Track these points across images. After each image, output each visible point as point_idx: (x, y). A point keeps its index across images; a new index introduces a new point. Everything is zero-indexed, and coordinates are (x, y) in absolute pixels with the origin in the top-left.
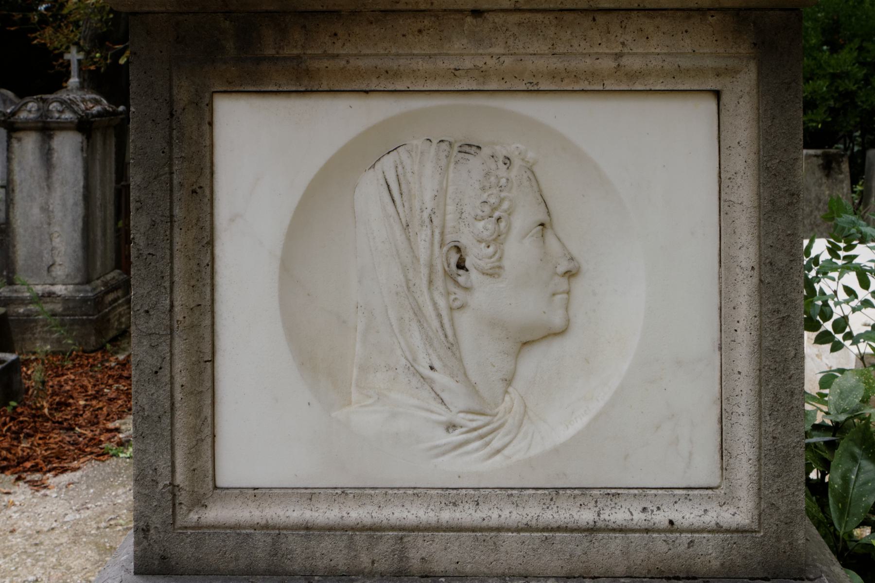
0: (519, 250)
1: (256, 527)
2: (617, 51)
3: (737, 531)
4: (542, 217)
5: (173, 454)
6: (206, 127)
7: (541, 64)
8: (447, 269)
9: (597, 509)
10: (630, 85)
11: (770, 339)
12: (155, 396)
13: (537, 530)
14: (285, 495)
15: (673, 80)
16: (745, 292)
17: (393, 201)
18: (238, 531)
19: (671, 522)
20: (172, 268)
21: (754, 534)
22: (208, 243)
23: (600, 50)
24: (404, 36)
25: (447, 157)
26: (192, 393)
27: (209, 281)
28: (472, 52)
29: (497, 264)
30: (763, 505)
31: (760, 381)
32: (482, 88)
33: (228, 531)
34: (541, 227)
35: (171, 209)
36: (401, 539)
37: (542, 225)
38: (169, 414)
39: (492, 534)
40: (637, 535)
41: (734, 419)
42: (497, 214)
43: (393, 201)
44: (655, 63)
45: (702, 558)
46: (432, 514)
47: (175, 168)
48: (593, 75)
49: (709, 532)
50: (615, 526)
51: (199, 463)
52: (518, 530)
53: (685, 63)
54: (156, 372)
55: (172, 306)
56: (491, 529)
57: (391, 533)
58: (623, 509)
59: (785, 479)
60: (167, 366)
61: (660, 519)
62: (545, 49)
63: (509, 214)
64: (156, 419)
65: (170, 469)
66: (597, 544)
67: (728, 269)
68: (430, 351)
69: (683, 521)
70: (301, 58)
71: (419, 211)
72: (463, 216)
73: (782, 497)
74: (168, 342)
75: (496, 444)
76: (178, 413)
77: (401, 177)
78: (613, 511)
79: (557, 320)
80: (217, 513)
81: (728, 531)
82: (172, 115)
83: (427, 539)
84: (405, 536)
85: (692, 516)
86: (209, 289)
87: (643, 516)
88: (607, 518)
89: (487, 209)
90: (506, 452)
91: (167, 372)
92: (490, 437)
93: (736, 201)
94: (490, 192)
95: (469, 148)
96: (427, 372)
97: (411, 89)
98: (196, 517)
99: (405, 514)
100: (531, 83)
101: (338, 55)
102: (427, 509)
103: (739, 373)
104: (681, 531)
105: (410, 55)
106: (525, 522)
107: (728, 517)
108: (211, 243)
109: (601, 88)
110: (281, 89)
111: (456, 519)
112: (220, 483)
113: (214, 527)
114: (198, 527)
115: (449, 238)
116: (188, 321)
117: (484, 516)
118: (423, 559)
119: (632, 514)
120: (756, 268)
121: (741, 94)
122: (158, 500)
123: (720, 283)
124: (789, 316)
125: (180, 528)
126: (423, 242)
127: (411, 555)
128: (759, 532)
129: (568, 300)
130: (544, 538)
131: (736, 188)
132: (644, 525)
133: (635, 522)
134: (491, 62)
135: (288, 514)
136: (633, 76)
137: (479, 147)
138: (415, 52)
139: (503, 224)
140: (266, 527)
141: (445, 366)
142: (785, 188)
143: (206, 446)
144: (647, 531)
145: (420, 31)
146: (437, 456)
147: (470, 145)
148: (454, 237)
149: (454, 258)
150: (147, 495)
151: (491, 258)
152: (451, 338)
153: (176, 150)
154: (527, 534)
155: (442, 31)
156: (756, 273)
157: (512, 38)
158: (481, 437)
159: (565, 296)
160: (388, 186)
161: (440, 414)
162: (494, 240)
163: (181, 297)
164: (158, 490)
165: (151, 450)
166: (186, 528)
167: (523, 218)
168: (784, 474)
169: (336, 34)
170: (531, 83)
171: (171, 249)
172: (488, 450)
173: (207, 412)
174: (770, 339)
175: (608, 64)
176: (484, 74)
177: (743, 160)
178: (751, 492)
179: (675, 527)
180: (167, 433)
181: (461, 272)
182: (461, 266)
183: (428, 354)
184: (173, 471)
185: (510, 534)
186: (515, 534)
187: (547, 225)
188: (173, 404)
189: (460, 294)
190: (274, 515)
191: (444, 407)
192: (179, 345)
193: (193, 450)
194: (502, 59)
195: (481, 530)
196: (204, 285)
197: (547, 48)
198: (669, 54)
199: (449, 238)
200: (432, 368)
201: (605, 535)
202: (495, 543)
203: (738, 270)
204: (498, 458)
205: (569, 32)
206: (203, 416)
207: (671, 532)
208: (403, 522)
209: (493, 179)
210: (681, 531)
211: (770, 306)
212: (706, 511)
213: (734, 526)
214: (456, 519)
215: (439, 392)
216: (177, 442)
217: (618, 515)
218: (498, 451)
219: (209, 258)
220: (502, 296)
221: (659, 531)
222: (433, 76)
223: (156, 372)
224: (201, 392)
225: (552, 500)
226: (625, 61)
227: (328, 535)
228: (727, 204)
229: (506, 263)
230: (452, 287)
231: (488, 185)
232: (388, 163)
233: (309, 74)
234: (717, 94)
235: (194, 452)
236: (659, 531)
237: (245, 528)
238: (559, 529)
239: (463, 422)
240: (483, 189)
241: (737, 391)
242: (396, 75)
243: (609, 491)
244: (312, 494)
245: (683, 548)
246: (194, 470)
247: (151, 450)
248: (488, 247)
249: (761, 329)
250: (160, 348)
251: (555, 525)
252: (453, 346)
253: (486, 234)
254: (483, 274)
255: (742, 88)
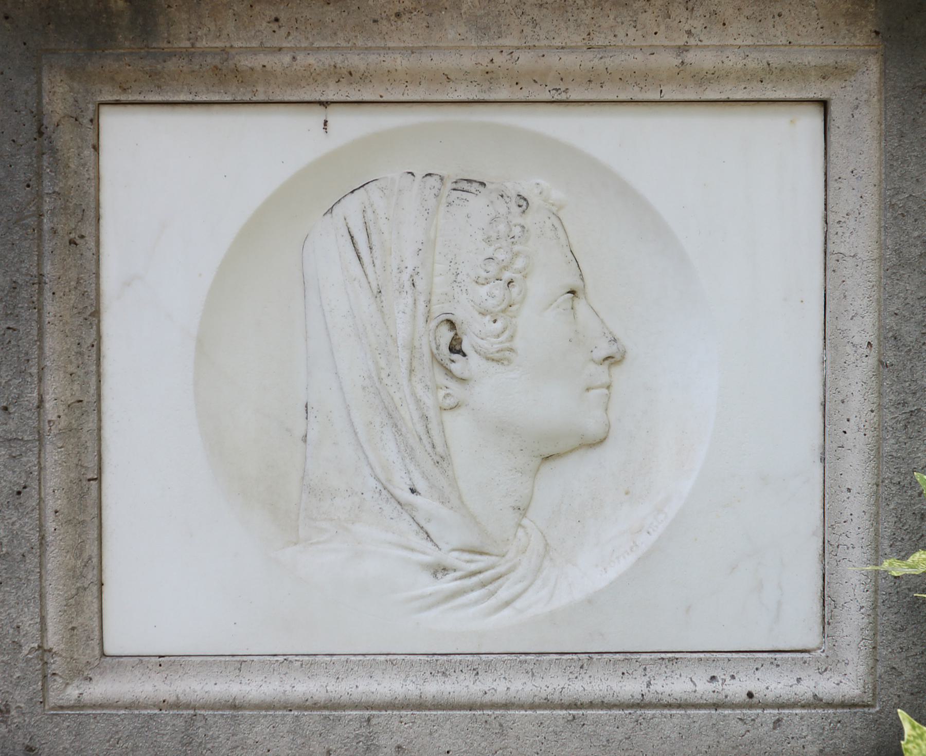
0: (539, 323)
1: (163, 705)
2: (681, 43)
3: (843, 705)
4: (572, 281)
5: (42, 607)
6: (88, 152)
7: (570, 60)
8: (435, 351)
9: (646, 679)
10: (701, 92)
11: (893, 441)
12: (18, 525)
13: (562, 706)
14: (201, 664)
15: (760, 84)
16: (858, 377)
17: (359, 258)
18: (136, 712)
19: (750, 695)
20: (41, 348)
21: (866, 710)
22: (92, 315)
23: (656, 41)
24: (375, 21)
25: (436, 196)
26: (69, 522)
27: (94, 368)
28: (474, 44)
29: (507, 345)
30: (880, 670)
31: (877, 500)
32: (486, 97)
33: (123, 712)
34: (570, 295)
35: (39, 265)
36: (369, 720)
37: (572, 292)
38: (37, 551)
39: (498, 712)
40: (702, 712)
41: (841, 552)
42: (507, 275)
43: (359, 258)
44: (733, 60)
45: (792, 741)
46: (411, 687)
47: (46, 207)
48: (644, 77)
49: (803, 707)
50: (671, 700)
51: (80, 620)
52: (533, 706)
53: (777, 59)
54: (19, 493)
55: (41, 401)
56: (494, 706)
57: (354, 713)
58: (683, 678)
59: (910, 634)
60: (35, 484)
61: (736, 689)
62: (577, 39)
63: (525, 277)
64: (19, 558)
65: (38, 626)
66: (644, 724)
67: (835, 347)
68: (412, 468)
69: (766, 692)
70: (227, 53)
71: (395, 271)
72: (459, 278)
73: (907, 658)
74: (36, 450)
75: (504, 594)
76: (50, 549)
77: (371, 225)
78: (669, 681)
79: (592, 425)
80: (102, 688)
81: (830, 705)
82: (41, 133)
83: (404, 720)
84: (374, 716)
85: (780, 686)
86: (94, 379)
87: (712, 686)
88: (660, 689)
89: (493, 268)
90: (518, 604)
91: (34, 493)
92: (496, 584)
93: (848, 254)
94: (498, 245)
95: (467, 185)
96: (407, 496)
97: (384, 99)
98: (77, 692)
99: (374, 687)
100: (557, 90)
101: (280, 49)
102: (405, 680)
103: (849, 490)
104: (765, 706)
105: (384, 48)
106: (544, 696)
107: (828, 686)
108: (97, 313)
109: (657, 97)
110: (197, 99)
111: (446, 693)
112: (109, 649)
113: (101, 706)
114: (79, 705)
115: (437, 309)
116: (63, 423)
117: (487, 689)
118: (399, 747)
119: (695, 685)
120: (875, 343)
121: (856, 102)
122: (22, 670)
123: (824, 369)
124: (919, 410)
125: (53, 708)
126: (401, 315)
127: (382, 742)
128: (873, 706)
129: (609, 397)
130: (570, 718)
131: (848, 234)
132: (712, 698)
133: (699, 696)
134: (500, 60)
135: (207, 688)
136: (703, 78)
137: (483, 184)
138: (390, 44)
139: (515, 290)
140: (177, 705)
141: (432, 486)
142: (916, 234)
143: (90, 597)
144: (716, 706)
145: (398, 15)
146: (421, 610)
147: (469, 181)
148: (447, 308)
149: (446, 336)
150: (7, 663)
151: (498, 336)
152: (440, 449)
153: (47, 183)
154: (547, 712)
155: (430, 15)
156: (874, 353)
157: (531, 24)
158: (483, 585)
159: (605, 391)
160: (352, 237)
161: (424, 553)
162: (504, 311)
163: (55, 388)
164: (21, 656)
165: (12, 600)
166: (62, 708)
167: (544, 283)
168: (910, 627)
169: (277, 20)
170: (557, 90)
171: (40, 321)
172: (493, 601)
173: (91, 549)
174: (893, 441)
175: (670, 60)
176: (490, 76)
177: (861, 199)
178: (863, 652)
179: (755, 700)
180: (34, 577)
181: (455, 357)
182: (455, 348)
183: (408, 472)
184: (43, 629)
185: (523, 712)
186: (529, 712)
187: (580, 294)
188: (42, 538)
189: (455, 388)
190: (188, 690)
191: (430, 544)
192: (52, 455)
193: (72, 601)
194: (515, 55)
195: (482, 707)
196: (87, 373)
197: (580, 38)
198: (755, 47)
199: (437, 309)
200: (413, 491)
201: (657, 712)
202: (501, 725)
203: (849, 349)
204: (507, 612)
205: (612, 17)
206: (85, 556)
207: (751, 707)
208: (372, 698)
209: (502, 227)
210: (765, 706)
211: (892, 397)
212: (799, 680)
213: (838, 698)
214: (446, 693)
215: (422, 523)
216: (49, 589)
217: (676, 685)
218: (507, 604)
219: (94, 336)
220: (512, 393)
221: (734, 706)
222: (414, 78)
223: (19, 493)
224: (83, 522)
225: (582, 667)
226: (690, 57)
227: (265, 716)
228: (835, 257)
229: (518, 344)
230: (441, 378)
231: (494, 235)
232: (352, 207)
233: (239, 76)
234: (824, 104)
235: (73, 604)
236: (734, 706)
237: (146, 708)
238: (591, 705)
239: (458, 564)
240: (488, 240)
241: (846, 514)
242: (365, 78)
243: (663, 655)
244: (242, 662)
245: (766, 729)
246: (73, 629)
247: (12, 600)
248: (495, 321)
249: (880, 427)
250: (24, 459)
251: (586, 700)
252: (442, 460)
253: (490, 303)
254: (488, 359)
255: (861, 94)
